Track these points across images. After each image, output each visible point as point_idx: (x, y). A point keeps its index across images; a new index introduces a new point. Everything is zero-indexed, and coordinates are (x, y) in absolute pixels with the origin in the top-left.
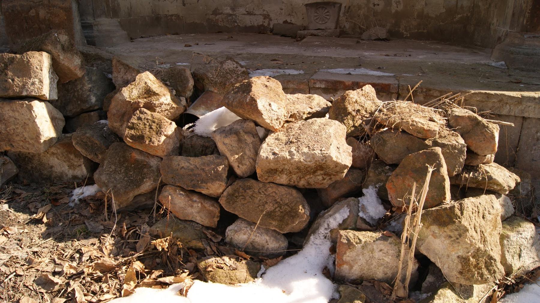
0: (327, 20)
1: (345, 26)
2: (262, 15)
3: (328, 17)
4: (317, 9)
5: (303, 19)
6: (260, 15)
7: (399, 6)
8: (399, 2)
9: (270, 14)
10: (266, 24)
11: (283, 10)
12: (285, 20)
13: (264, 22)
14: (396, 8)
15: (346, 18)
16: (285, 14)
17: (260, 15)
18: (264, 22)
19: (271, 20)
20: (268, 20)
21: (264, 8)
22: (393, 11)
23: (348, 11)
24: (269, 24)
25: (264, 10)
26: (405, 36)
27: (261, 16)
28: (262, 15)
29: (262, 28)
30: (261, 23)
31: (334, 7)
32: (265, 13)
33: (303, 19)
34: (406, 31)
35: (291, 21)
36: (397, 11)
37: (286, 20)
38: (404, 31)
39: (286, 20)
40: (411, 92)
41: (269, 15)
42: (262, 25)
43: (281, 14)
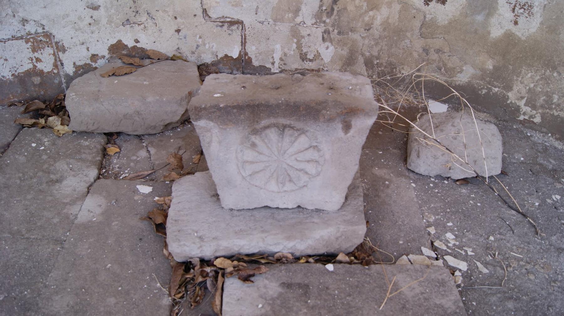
0: (305, 178)
1: (318, 56)
2: (21, 38)
3: (311, 168)
4: (255, 132)
5: (178, 31)
6: (14, 38)
7: (521, 20)
8: (528, 8)
9: (54, 32)
10: (46, 66)
11: (102, 10)
12: (114, 41)
13: (38, 60)
14: (511, 27)
15: (327, 32)
16: (110, 22)
17: (14, 38)
18: (38, 60)
19: (60, 48)
20: (50, 51)
21: (21, 14)
22: (496, 33)
23: (333, 9)
24: (59, 63)
25: (24, 21)
26: (522, 118)
27: (21, 43)
28: (21, 38)
29: (37, 80)
30: (28, 66)
31: (347, 127)
32: (31, 28)
33: (178, 31)
34: (531, 103)
35: (137, 41)
36: (509, 37)
37: (120, 42)
38: (522, 103)
39: (120, 42)
40: (414, 83)
41: (48, 35)
42: (34, 72)
43: (95, 22)
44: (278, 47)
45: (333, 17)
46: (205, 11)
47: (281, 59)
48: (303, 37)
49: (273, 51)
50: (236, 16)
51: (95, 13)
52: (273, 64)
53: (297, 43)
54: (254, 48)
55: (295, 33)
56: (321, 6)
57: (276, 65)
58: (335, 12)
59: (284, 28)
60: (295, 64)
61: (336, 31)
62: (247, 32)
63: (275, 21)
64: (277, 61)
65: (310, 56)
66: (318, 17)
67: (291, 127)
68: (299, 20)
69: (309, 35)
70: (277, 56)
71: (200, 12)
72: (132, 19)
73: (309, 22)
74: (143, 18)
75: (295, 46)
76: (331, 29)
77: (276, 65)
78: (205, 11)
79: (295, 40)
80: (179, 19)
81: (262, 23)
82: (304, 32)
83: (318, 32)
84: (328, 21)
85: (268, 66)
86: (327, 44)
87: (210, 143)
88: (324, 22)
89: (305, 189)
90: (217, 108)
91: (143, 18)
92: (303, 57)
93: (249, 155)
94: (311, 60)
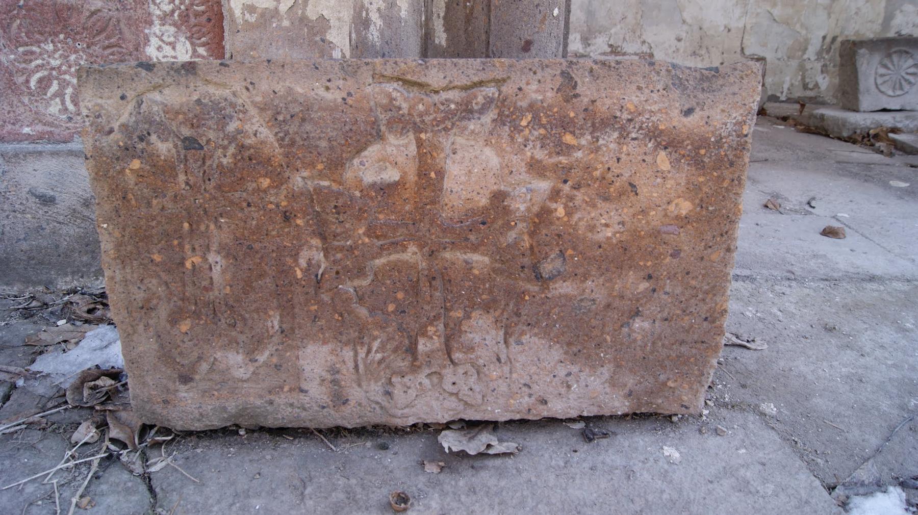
1: (817, 85)
15: (825, 66)
16: (684, 52)
21: (644, 37)
44: (788, 79)
45: (831, 54)
46: (742, 49)
47: (789, 89)
48: (807, 70)
49: (783, 82)
50: (762, 54)
51: (679, 44)
52: (782, 93)
53: (802, 75)
54: (770, 80)
55: (802, 68)
56: (822, 46)
57: (784, 94)
58: (832, 50)
59: (794, 63)
60: (798, 93)
61: (832, 65)
62: (767, 67)
63: (789, 58)
64: (785, 90)
65: (811, 86)
66: (819, 55)
67: (907, 53)
68: (806, 57)
69: (811, 69)
70: (786, 86)
71: (739, 50)
72: (697, 52)
73: (813, 58)
74: (703, 52)
75: (800, 78)
76: (828, 63)
77: (784, 94)
78: (742, 49)
79: (801, 73)
80: (725, 55)
81: (779, 59)
82: (808, 66)
83: (818, 66)
84: (826, 57)
85: (779, 95)
86: (825, 75)
87: (862, 65)
88: (824, 58)
89: (907, 95)
90: (270, 429)
91: (703, 52)
92: (805, 87)
93: (882, 71)
94: (811, 89)
